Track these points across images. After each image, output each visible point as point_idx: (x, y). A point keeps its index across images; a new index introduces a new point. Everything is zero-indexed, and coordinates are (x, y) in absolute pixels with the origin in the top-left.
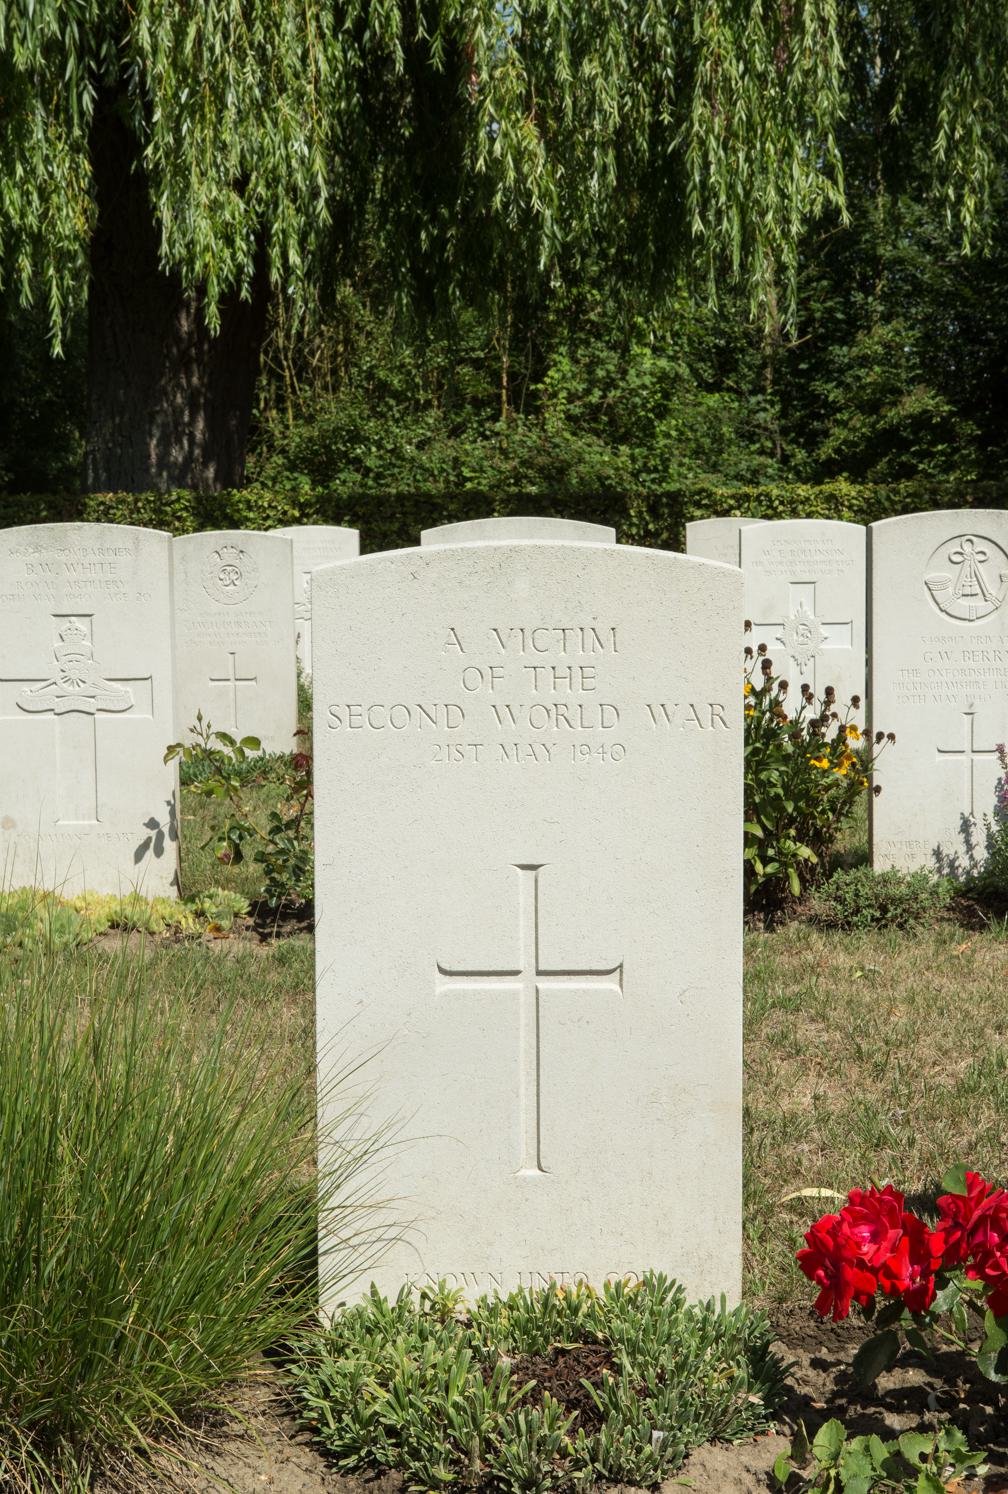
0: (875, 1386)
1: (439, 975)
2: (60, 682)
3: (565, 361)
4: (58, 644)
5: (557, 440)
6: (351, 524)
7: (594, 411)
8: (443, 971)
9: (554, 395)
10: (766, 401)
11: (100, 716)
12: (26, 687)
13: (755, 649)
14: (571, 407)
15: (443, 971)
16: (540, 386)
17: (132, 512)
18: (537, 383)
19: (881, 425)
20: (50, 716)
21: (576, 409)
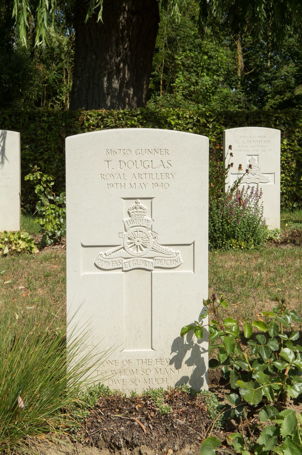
0: (200, 356)
1: (82, 248)
2: (127, 246)
3: (181, 76)
4: (127, 218)
5: (181, 102)
6: (276, 127)
7: (191, 94)
8: (83, 246)
9: (178, 88)
10: (240, 91)
11: (155, 271)
12: (102, 251)
13: (250, 169)
14: (184, 91)
15: (83, 246)
16: (174, 84)
17: (116, 120)
18: (173, 83)
19: (286, 98)
20: (119, 272)
21: (186, 92)
